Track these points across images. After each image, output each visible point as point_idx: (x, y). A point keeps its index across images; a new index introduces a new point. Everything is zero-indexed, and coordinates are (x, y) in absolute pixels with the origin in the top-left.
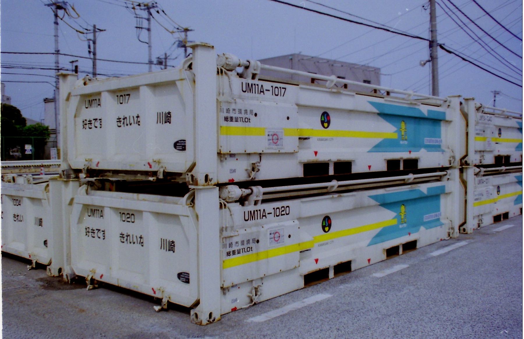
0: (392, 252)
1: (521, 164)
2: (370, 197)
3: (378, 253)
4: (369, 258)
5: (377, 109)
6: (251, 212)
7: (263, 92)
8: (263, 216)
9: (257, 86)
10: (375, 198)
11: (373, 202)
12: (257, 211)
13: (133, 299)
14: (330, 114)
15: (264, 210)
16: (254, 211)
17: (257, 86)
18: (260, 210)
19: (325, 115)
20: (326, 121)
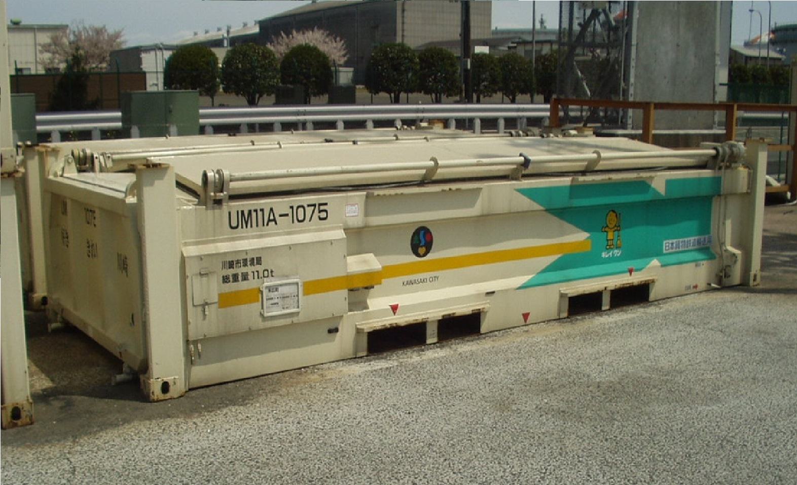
0: (583, 305)
1: (769, 2)
2: (522, 191)
3: (548, 300)
4: (526, 311)
5: (541, 205)
6: (243, 212)
7: (274, 220)
8: (269, 220)
9: (260, 213)
10: (529, 193)
11: (526, 203)
12: (256, 211)
13: (27, 25)
14: (431, 230)
15: (271, 210)
16: (250, 212)
17: (260, 213)
18: (262, 210)
19: (422, 233)
20: (423, 243)
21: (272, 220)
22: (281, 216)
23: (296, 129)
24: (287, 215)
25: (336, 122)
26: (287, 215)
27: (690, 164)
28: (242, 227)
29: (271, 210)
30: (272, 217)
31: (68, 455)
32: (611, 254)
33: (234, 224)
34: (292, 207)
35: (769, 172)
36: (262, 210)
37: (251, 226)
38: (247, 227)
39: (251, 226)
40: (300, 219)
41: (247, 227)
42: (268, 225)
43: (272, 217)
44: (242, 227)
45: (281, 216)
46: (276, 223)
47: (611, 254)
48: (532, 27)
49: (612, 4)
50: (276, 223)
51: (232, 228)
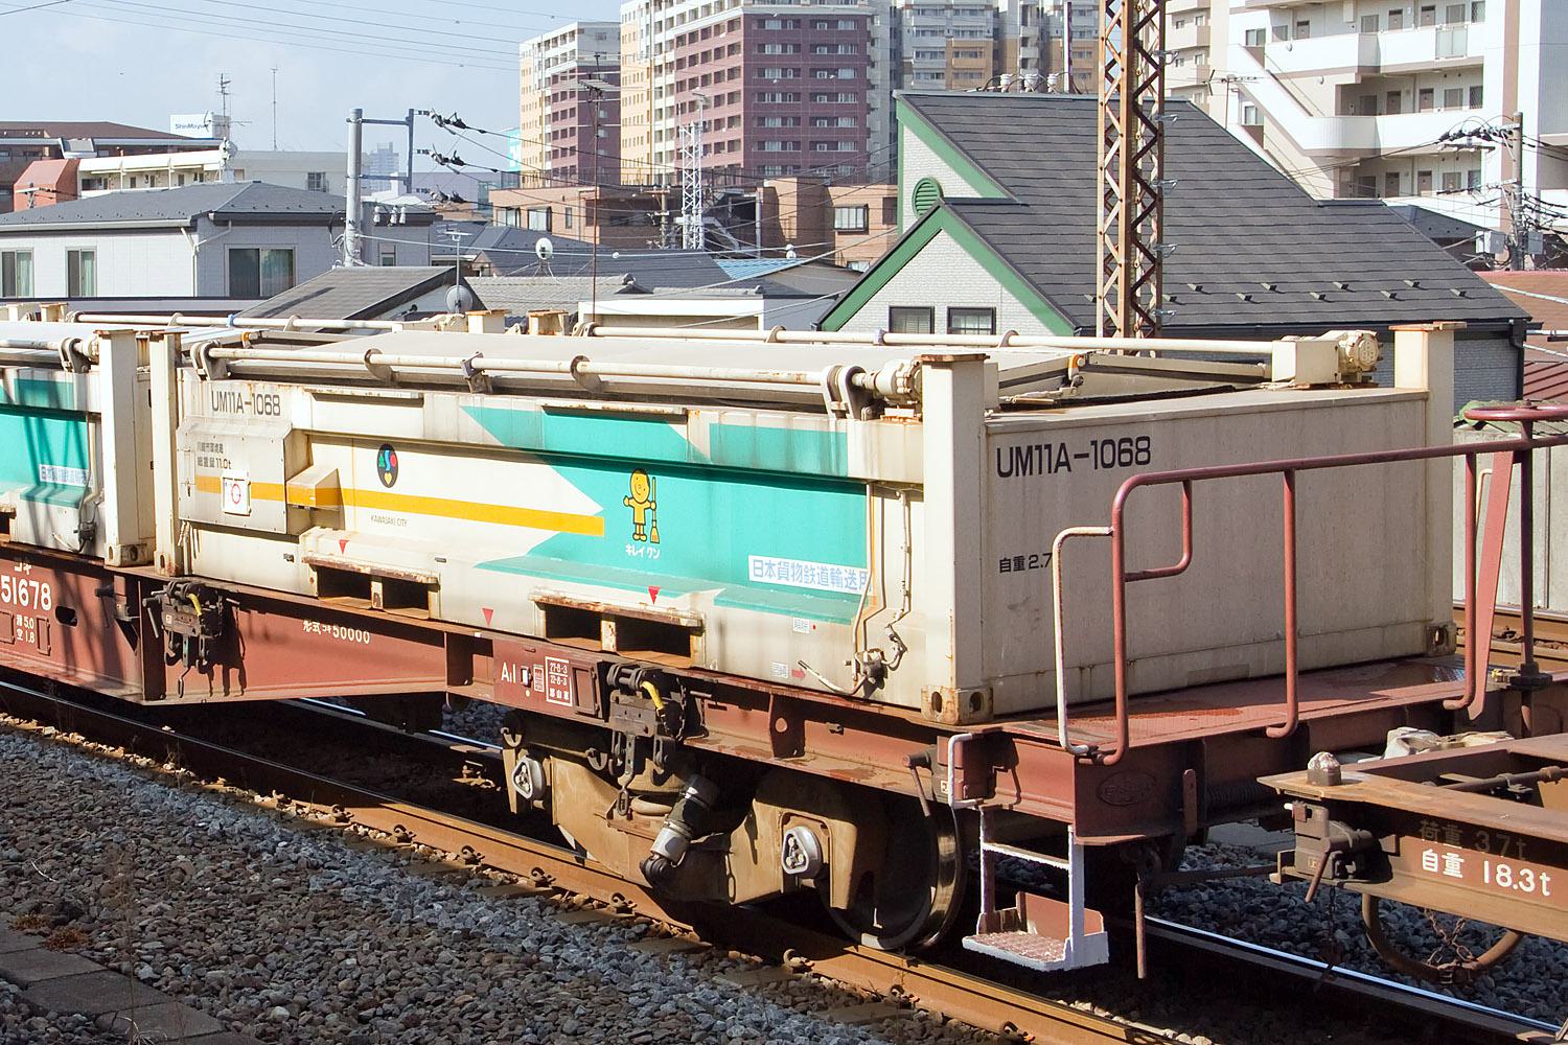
7: (1067, 464)
8: (1059, 464)
9: (1045, 452)
12: (1039, 448)
15: (1063, 446)
16: (1030, 448)
17: (1045, 452)
18: (1048, 447)
21: (1063, 464)
22: (1076, 456)
23: (1361, 684)
24: (1087, 455)
25: (1372, 896)
26: (1087, 455)
27: (656, 811)
28: (1017, 475)
29: (1063, 446)
30: (1063, 459)
31: (357, 992)
32: (641, 551)
33: (1005, 469)
34: (1094, 443)
35: (584, 752)
36: (1048, 447)
37: (1031, 473)
38: (1024, 474)
39: (1031, 473)
40: (1106, 462)
41: (1024, 474)
42: (1056, 471)
43: (1063, 459)
44: (1017, 475)
45: (1076, 456)
46: (1069, 470)
47: (641, 551)
48: (1129, 720)
49: (1298, 474)
50: (1069, 470)
51: (1002, 474)
